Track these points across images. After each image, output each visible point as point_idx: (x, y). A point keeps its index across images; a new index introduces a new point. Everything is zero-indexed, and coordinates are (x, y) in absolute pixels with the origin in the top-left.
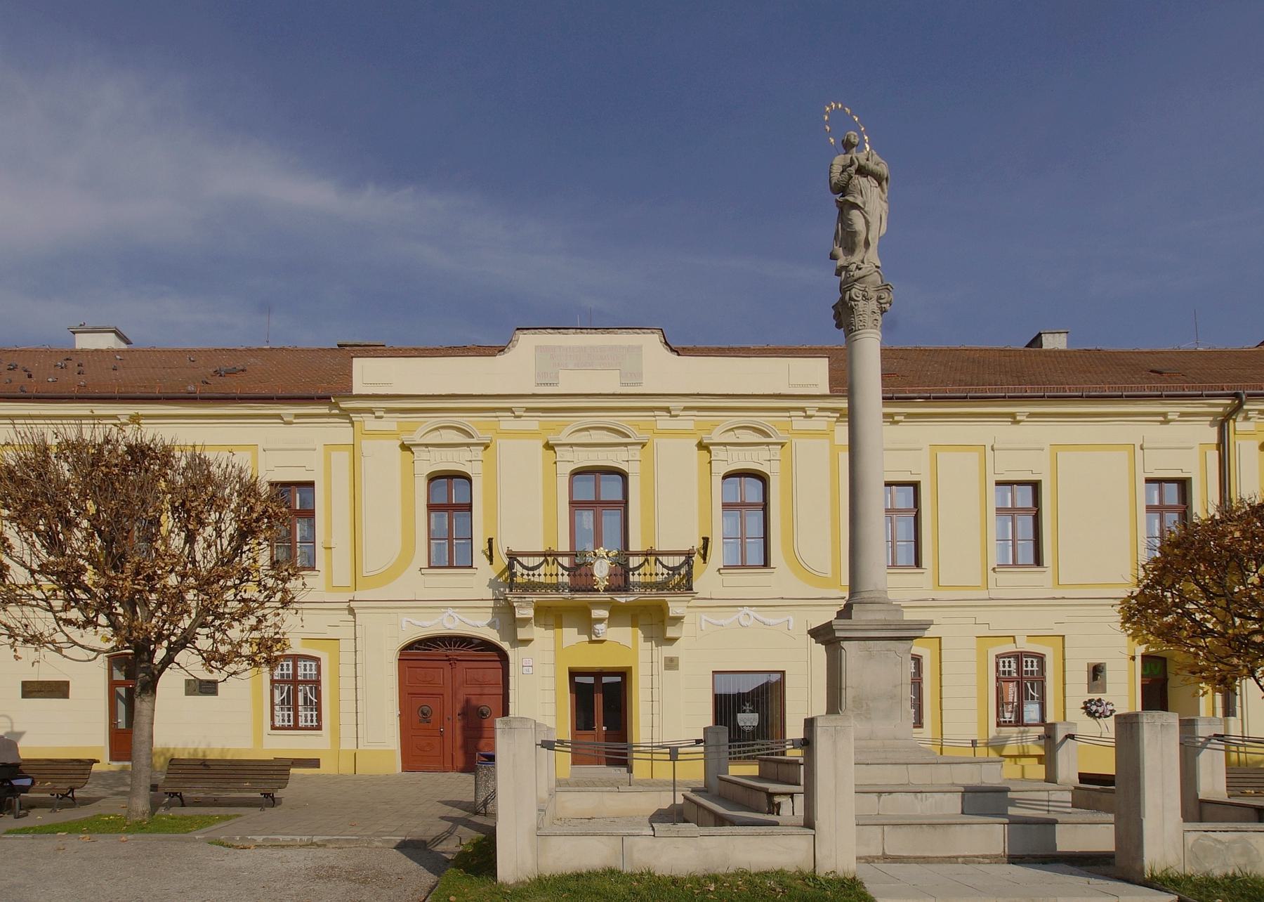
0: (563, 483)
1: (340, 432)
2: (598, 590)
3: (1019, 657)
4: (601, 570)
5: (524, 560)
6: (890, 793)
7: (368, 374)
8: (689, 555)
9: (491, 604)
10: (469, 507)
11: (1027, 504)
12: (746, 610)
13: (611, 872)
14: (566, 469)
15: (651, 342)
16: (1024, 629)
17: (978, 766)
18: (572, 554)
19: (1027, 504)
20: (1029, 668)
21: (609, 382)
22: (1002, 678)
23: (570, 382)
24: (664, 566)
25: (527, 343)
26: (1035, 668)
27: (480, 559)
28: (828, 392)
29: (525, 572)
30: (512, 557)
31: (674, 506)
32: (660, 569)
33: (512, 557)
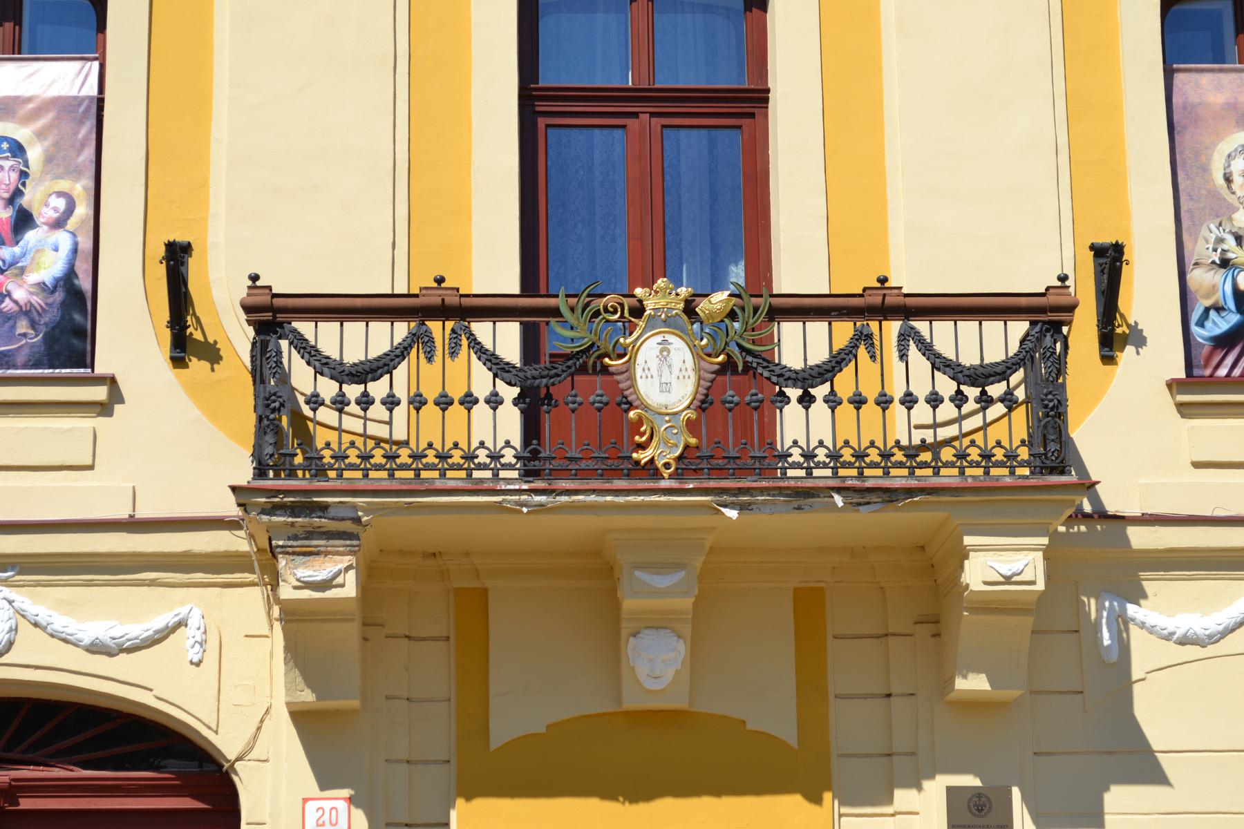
2: (650, 470)
5: (326, 336)
24: (939, 363)
29: (328, 388)
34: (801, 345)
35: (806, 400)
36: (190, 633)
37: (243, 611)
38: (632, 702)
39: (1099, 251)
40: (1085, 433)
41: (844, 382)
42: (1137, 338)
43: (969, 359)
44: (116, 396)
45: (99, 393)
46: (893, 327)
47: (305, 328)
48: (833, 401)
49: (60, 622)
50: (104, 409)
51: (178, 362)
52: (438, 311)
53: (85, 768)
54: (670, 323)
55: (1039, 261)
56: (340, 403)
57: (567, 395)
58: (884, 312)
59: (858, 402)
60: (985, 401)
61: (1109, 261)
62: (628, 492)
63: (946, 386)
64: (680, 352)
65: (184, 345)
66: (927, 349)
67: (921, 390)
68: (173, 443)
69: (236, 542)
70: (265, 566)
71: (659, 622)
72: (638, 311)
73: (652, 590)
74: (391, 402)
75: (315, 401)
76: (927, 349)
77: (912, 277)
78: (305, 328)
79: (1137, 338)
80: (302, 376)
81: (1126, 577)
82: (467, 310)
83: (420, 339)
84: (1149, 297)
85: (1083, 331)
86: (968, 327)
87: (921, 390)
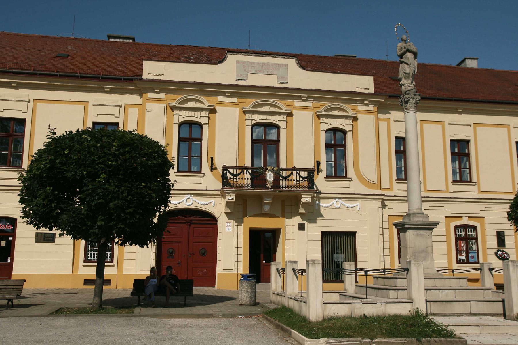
0: (248, 130)
1: (135, 99)
2: (268, 188)
3: (466, 227)
4: (270, 177)
5: (232, 171)
6: (430, 290)
7: (151, 69)
8: (311, 172)
9: (172, 192)
10: (200, 140)
11: (460, 150)
12: (337, 200)
13: (351, 318)
14: (250, 123)
15: (292, 63)
16: (466, 212)
17: (458, 280)
18: (252, 168)
19: (460, 150)
20: (93, 252)
21: (271, 81)
22: (458, 239)
23: (254, 80)
24: (300, 176)
25: (232, 59)
26: (89, 252)
27: (205, 167)
28: (372, 91)
29: (232, 177)
30: (226, 168)
31: (302, 145)
32: (298, 178)
33: (226, 168)
34: (284, 174)
35: (285, 180)
36: (213, 203)
37: (219, 200)
38: (263, 212)
39: (317, 162)
40: (316, 182)
41: (290, 178)
42: (321, 171)
43: (304, 176)
44: (205, 175)
45: (203, 175)
46: (295, 172)
47: (230, 170)
48: (288, 180)
49: (198, 201)
50: (203, 176)
51: (211, 171)
52: (243, 168)
53: (390, 337)
54: (271, 171)
55: (311, 165)
56: (233, 178)
57: (258, 178)
58: (294, 170)
59: (291, 180)
60: (305, 181)
61: (318, 163)
62: (355, 341)
63: (301, 179)
64: (272, 174)
65: (213, 168)
66: (299, 175)
67: (298, 179)
68: (211, 181)
69: (219, 193)
70: (223, 196)
71: (267, 203)
72: (267, 169)
73: (268, 200)
74: (239, 179)
75: (231, 178)
76: (299, 175)
77: (298, 167)
78: (230, 170)
79: (321, 171)
80: (229, 175)
81: (319, 198)
82: (248, 168)
83: (243, 172)
84: (323, 166)
85: (315, 173)
86: (303, 172)
87: (298, 179)
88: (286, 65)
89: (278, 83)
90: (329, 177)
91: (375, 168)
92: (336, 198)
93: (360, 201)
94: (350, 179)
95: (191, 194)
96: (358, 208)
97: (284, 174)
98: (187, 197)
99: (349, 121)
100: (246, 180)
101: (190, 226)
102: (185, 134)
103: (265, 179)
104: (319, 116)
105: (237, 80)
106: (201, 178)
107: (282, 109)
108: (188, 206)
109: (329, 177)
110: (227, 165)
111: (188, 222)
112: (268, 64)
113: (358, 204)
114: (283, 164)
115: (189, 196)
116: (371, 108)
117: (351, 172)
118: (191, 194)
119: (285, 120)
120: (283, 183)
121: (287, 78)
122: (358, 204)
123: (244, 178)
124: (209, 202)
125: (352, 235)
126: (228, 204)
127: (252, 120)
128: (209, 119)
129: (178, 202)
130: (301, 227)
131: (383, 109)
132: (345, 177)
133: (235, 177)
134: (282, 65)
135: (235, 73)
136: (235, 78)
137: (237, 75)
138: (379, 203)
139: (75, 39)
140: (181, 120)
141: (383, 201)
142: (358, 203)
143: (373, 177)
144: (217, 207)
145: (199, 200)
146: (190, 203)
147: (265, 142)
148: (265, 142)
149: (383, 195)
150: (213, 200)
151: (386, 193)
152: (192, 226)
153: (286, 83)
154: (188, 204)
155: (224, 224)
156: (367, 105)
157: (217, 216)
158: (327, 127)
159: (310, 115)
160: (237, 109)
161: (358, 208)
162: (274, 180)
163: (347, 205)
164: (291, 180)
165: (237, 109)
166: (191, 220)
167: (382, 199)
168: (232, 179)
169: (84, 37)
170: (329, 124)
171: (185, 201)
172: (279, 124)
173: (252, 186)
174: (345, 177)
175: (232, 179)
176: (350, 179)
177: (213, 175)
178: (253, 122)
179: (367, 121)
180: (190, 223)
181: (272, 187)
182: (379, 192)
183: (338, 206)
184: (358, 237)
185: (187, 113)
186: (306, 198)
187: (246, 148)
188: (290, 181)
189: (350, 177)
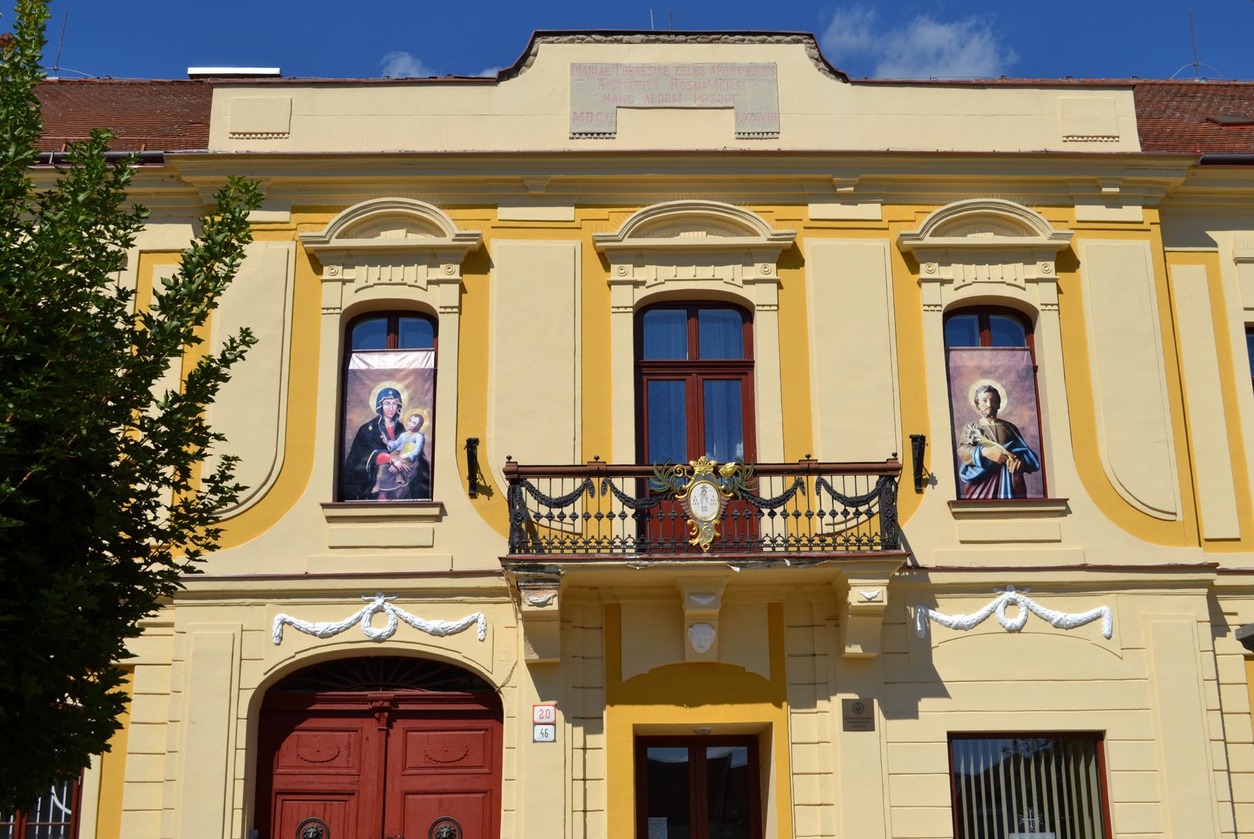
0: (623, 328)
2: (698, 548)
5: (543, 485)
14: (628, 297)
21: (713, 133)
23: (638, 133)
24: (836, 496)
27: (449, 481)
28: (1131, 143)
29: (544, 510)
30: (517, 476)
32: (826, 502)
35: (772, 514)
36: (479, 626)
37: (505, 613)
38: (690, 659)
40: (910, 527)
41: (790, 506)
42: (933, 481)
44: (443, 512)
45: (436, 511)
47: (533, 481)
48: (785, 515)
49: (418, 620)
50: (438, 518)
52: (596, 473)
56: (550, 517)
57: (658, 516)
63: (839, 507)
65: (476, 487)
66: (830, 489)
67: (827, 509)
68: (470, 535)
70: (515, 594)
71: (703, 620)
72: (691, 472)
73: (697, 606)
74: (574, 517)
75: (538, 516)
76: (830, 489)
77: (822, 456)
78: (533, 481)
79: (933, 481)
80: (532, 503)
83: (588, 486)
85: (906, 480)
86: (849, 479)
87: (827, 509)
88: (772, 68)
89: (741, 136)
90: (963, 502)
91: (1168, 455)
92: (1003, 587)
93: (1112, 596)
94: (1061, 508)
95: (387, 593)
96: (1105, 626)
97: (770, 487)
98: (372, 606)
99: (1044, 269)
100: (617, 520)
101: (390, 725)
102: (673, 344)
103: (684, 514)
104: (912, 258)
105: (576, 135)
106: (429, 525)
107: (755, 234)
108: (378, 639)
109: (963, 502)
110: (523, 460)
111: (381, 710)
112: (698, 69)
113: (1104, 609)
114: (769, 450)
115: (379, 601)
116: (1133, 213)
117: (1062, 477)
118: (387, 593)
119: (773, 276)
120: (771, 527)
121: (775, 117)
122: (1104, 609)
123: (593, 512)
124: (464, 621)
125: (1086, 746)
126: (530, 621)
127: (636, 284)
128: (463, 290)
129: (335, 625)
130: (858, 719)
131: (1184, 227)
132: (1045, 500)
133: (556, 512)
134: (752, 69)
135: (567, 110)
136: (566, 128)
137: (575, 117)
138: (1197, 603)
139: (61, 82)
140: (351, 298)
141: (1214, 594)
142: (1102, 605)
143: (1163, 491)
144: (491, 641)
145: (420, 613)
146: (386, 630)
147: (693, 365)
148: (693, 365)
149: (1212, 567)
150: (479, 612)
151: (1227, 559)
152: (400, 725)
153: (774, 134)
154: (376, 632)
155: (525, 709)
156: (1113, 202)
157: (497, 679)
158: (950, 296)
159: (878, 252)
160: (575, 243)
161: (1105, 626)
162: (724, 516)
163: (1057, 615)
164: (797, 515)
165: (575, 243)
166: (395, 701)
167: (1208, 584)
168: (544, 521)
169: (92, 78)
170: (957, 284)
171: (364, 623)
172: (752, 294)
173: (642, 545)
174: (1045, 500)
175: (544, 521)
176: (1061, 508)
177: (480, 509)
178: (642, 293)
179: (1118, 254)
180: (392, 714)
181: (715, 546)
182: (1194, 555)
183: (1017, 621)
184: (1113, 753)
185: (375, 273)
186: (866, 592)
187: (615, 397)
188: (791, 519)
189: (1059, 496)
